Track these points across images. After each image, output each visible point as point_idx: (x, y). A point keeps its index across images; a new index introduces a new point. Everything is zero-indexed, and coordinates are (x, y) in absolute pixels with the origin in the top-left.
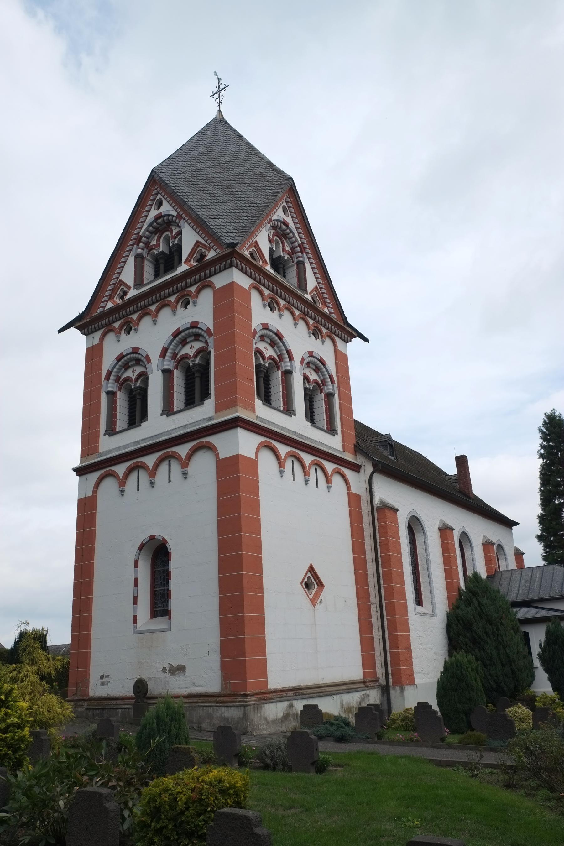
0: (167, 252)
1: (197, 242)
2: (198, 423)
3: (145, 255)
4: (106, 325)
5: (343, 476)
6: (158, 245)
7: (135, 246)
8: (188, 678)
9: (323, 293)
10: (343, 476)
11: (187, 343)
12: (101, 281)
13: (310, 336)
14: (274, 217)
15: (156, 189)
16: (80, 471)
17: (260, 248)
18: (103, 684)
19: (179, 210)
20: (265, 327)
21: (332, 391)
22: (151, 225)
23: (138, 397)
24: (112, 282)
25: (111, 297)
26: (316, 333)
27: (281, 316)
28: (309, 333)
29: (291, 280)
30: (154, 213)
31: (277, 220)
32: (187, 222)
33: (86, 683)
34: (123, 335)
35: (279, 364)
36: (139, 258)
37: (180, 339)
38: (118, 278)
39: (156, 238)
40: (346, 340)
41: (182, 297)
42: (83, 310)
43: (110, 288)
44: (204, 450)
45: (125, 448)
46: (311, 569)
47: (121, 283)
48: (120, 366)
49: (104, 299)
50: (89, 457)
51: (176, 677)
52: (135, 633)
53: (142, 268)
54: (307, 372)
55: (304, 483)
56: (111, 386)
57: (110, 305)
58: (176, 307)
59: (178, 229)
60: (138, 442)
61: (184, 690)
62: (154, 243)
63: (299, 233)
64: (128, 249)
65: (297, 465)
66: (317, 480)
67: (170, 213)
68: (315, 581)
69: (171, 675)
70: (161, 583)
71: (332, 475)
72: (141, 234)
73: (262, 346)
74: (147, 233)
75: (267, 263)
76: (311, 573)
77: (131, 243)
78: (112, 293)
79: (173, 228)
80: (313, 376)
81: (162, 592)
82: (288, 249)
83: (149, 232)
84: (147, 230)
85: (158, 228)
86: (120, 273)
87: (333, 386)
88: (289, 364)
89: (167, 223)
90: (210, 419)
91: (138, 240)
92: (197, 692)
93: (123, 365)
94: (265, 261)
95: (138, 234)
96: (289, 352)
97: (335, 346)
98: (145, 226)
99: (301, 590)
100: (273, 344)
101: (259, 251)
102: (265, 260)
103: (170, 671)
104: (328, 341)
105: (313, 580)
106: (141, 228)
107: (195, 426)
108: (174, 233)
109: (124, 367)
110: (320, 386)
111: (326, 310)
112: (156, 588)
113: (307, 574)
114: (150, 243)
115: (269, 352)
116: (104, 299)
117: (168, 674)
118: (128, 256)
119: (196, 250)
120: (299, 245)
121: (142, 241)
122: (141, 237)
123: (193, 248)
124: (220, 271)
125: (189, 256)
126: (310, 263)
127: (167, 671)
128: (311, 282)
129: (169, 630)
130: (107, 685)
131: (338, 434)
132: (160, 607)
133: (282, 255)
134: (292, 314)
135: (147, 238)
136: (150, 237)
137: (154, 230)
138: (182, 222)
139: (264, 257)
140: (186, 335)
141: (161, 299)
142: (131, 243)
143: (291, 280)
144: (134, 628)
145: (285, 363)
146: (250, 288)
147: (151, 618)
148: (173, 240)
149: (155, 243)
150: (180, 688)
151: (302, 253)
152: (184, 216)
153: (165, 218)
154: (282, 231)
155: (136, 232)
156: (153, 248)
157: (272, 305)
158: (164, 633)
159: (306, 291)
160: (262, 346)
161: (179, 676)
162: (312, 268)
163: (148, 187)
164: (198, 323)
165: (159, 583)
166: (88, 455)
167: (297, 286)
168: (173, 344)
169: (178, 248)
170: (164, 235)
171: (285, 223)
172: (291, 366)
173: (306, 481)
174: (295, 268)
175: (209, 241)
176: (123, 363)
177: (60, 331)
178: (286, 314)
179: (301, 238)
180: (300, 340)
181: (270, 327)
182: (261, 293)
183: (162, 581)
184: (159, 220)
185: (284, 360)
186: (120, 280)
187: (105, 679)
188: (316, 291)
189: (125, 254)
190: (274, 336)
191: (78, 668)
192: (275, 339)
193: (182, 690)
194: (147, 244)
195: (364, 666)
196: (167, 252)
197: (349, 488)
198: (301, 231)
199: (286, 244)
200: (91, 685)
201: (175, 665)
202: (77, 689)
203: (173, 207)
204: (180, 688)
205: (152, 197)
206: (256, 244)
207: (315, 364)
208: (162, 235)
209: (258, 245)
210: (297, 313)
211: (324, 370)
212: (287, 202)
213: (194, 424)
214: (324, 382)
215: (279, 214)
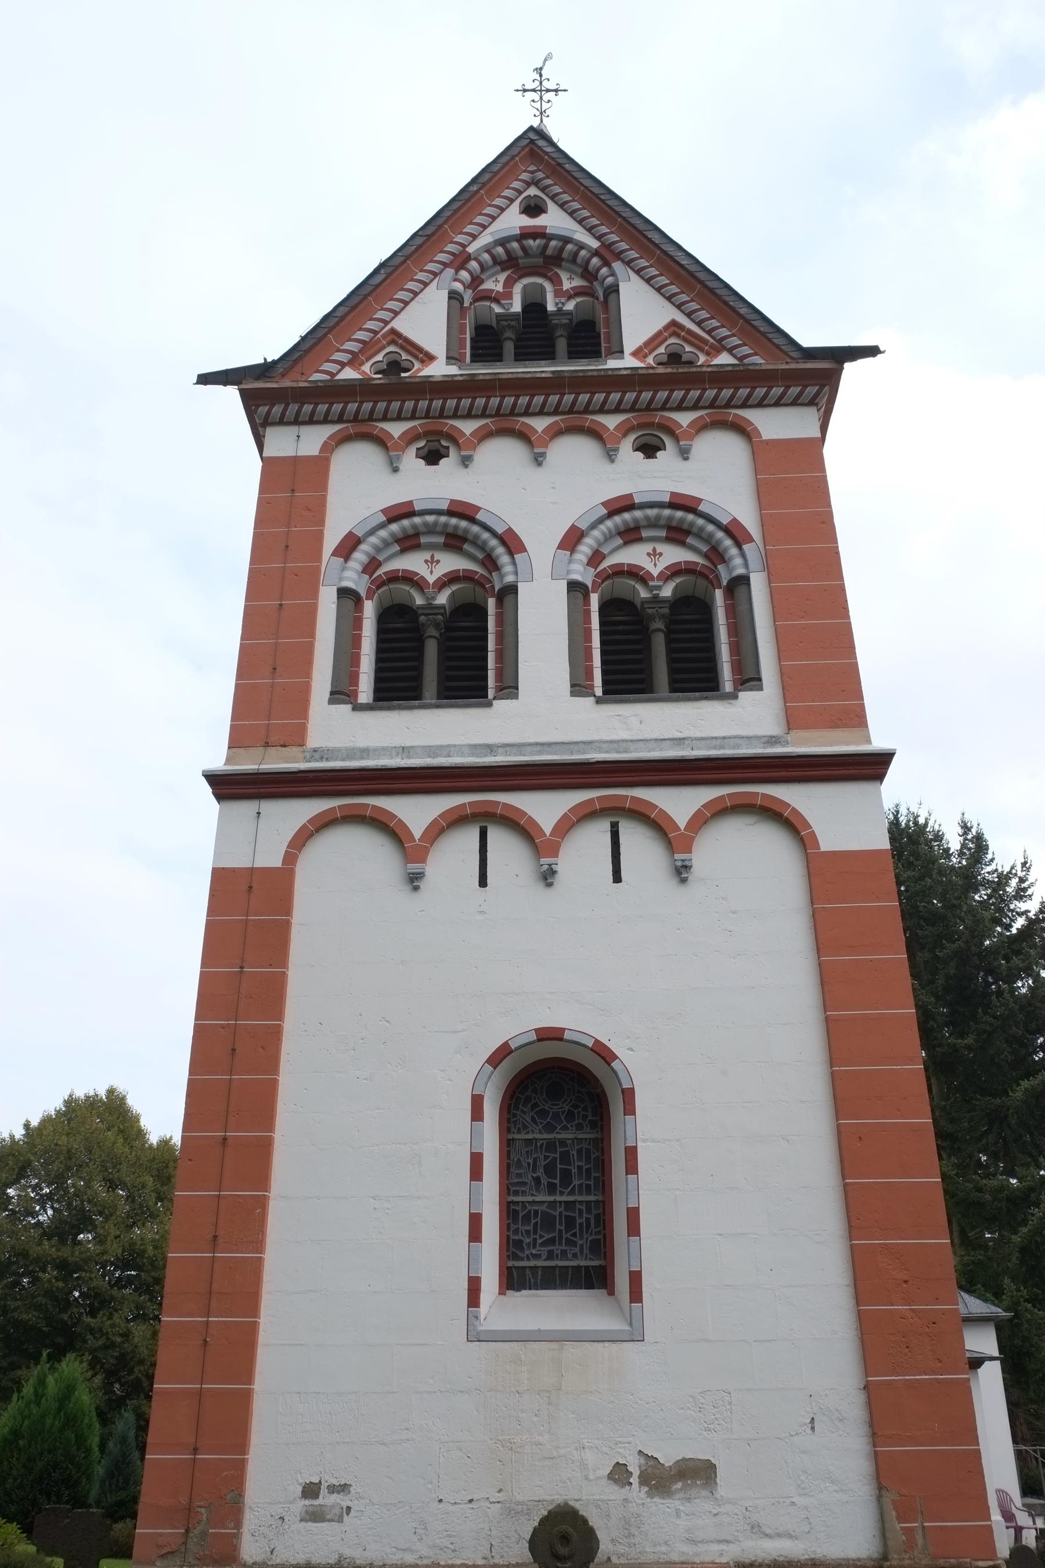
2: (732, 742)
4: (356, 419)
8: (728, 1508)
11: (640, 540)
12: (343, 310)
16: (225, 786)
18: (315, 1516)
22: (503, 242)
23: (432, 631)
24: (370, 325)
25: (355, 361)
30: (513, 221)
33: (232, 1508)
34: (411, 461)
37: (625, 522)
41: (641, 426)
42: (274, 355)
43: (360, 335)
44: (750, 819)
45: (435, 755)
48: (393, 535)
49: (338, 356)
50: (272, 751)
51: (674, 1503)
52: (474, 1336)
56: (353, 578)
57: (349, 374)
60: (491, 748)
61: (715, 1547)
69: (650, 1495)
70: (537, 1180)
72: (471, 249)
74: (486, 257)
77: (442, 257)
78: (361, 351)
81: (544, 1207)
83: (493, 257)
84: (488, 249)
85: (517, 258)
86: (396, 313)
89: (546, 257)
90: (772, 740)
91: (461, 261)
92: (774, 1555)
93: (400, 535)
95: (464, 246)
103: (644, 1480)
106: (474, 237)
107: (722, 747)
109: (449, 535)
112: (516, 1193)
114: (482, 282)
116: (338, 356)
117: (636, 1492)
121: (468, 266)
122: (469, 258)
123: (659, 333)
124: (778, 403)
125: (647, 344)
127: (634, 1480)
129: (635, 1336)
130: (340, 1520)
132: (537, 1257)
135: (483, 268)
136: (488, 268)
140: (647, 518)
141: (571, 411)
142: (442, 257)
144: (472, 1319)
147: (502, 1293)
150: (693, 1542)
153: (553, 243)
155: (460, 238)
158: (615, 1347)
161: (689, 1500)
165: (528, 1179)
166: (267, 745)
168: (602, 527)
170: (539, 280)
176: (404, 530)
177: (205, 379)
183: (540, 1173)
184: (531, 242)
187: (326, 1499)
189: (421, 276)
191: (195, 1451)
193: (702, 1548)
194: (476, 281)
195: (886, 1475)
200: (251, 1520)
201: (668, 1456)
202: (187, 1531)
204: (693, 1542)
205: (516, 184)
213: (718, 743)
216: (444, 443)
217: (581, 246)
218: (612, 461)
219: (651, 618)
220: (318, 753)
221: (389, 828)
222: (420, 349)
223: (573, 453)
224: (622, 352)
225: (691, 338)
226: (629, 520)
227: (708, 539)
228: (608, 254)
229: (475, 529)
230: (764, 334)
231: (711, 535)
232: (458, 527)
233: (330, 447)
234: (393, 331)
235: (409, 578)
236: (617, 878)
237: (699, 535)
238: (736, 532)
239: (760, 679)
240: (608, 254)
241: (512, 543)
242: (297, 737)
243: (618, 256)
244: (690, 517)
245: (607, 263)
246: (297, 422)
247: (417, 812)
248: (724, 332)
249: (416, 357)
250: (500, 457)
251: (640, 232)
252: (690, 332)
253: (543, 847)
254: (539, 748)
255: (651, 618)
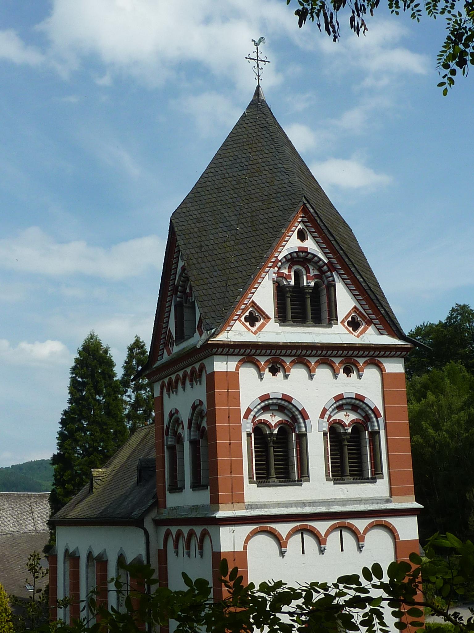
91: (275, 265)
184: (301, 253)
216: (278, 366)
217: (320, 260)
218: (336, 378)
219: (344, 440)
220: (250, 507)
221: (276, 536)
222: (264, 313)
223: (323, 373)
224: (337, 320)
225: (361, 314)
226: (342, 403)
227: (366, 412)
228: (331, 267)
229: (291, 406)
230: (389, 324)
231: (367, 411)
232: (284, 405)
233: (237, 368)
234: (253, 302)
235: (265, 423)
236: (342, 550)
237: (363, 409)
238: (375, 411)
239: (382, 474)
240: (331, 267)
241: (304, 415)
242: (241, 499)
243: (335, 269)
244: (361, 403)
245: (329, 270)
246: (226, 354)
247: (283, 529)
248: (373, 317)
249: (262, 316)
250: (298, 373)
251: (347, 265)
252: (360, 312)
253: (320, 541)
254: (319, 504)
255: (344, 440)
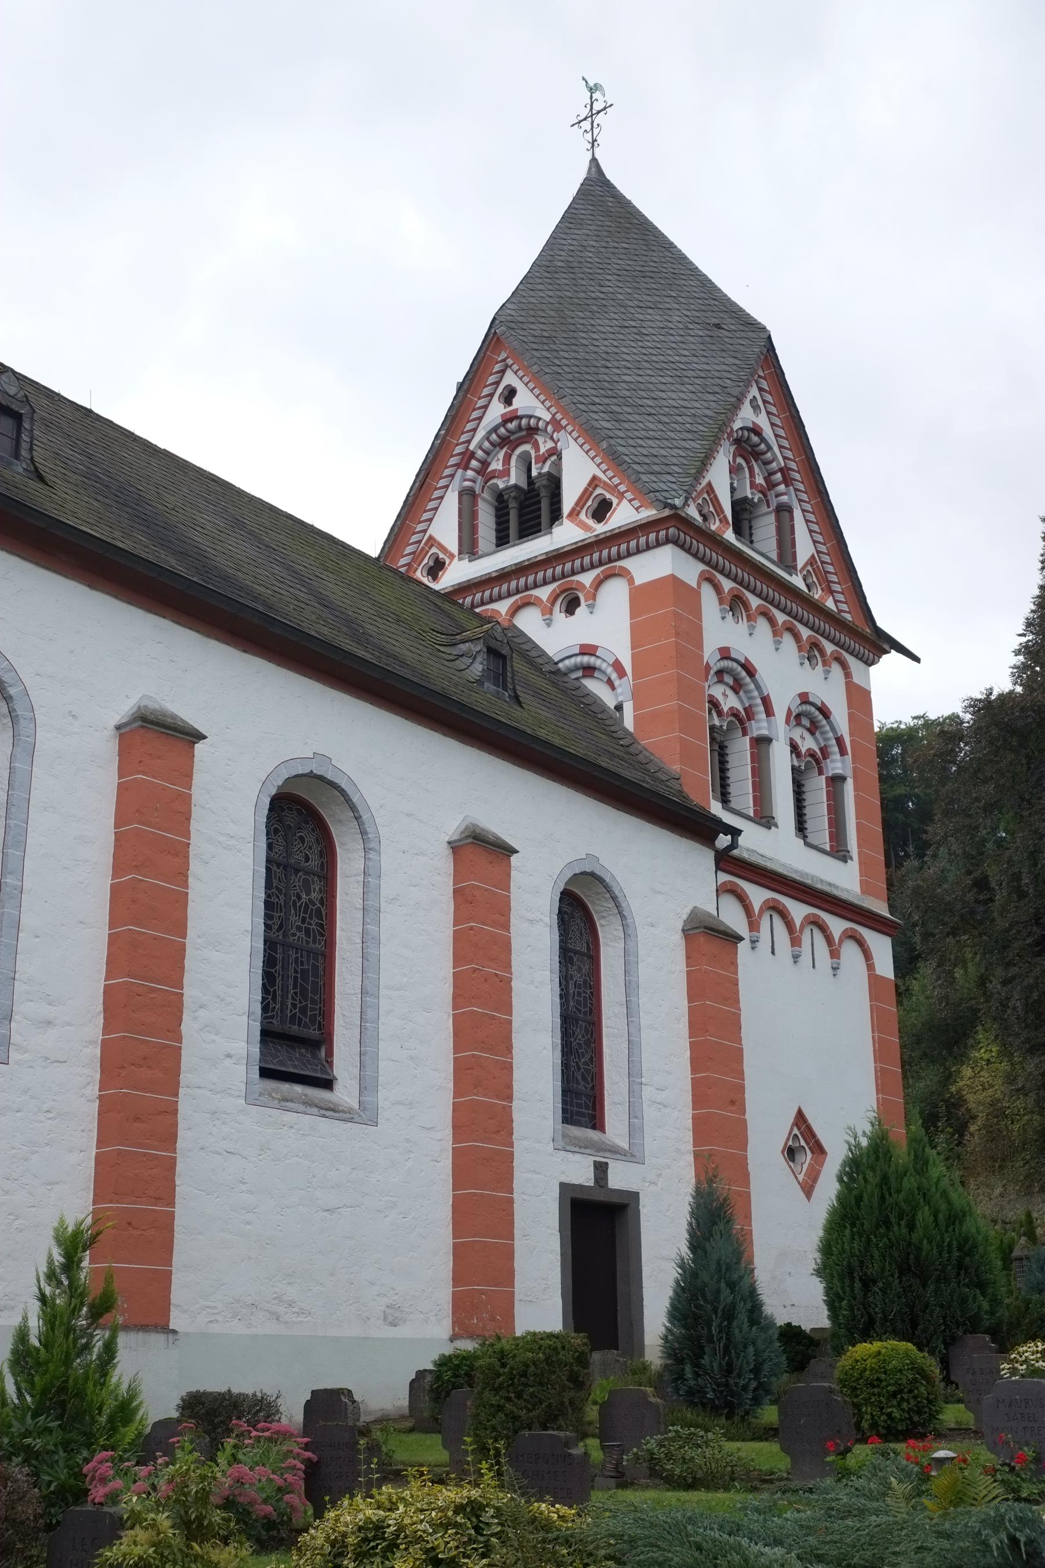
0: (524, 484)
1: (594, 478)
3: (478, 491)
5: (861, 943)
6: (506, 473)
7: (460, 471)
9: (822, 562)
10: (861, 943)
13: (802, 664)
14: (737, 425)
15: (504, 360)
17: (716, 496)
19: (553, 410)
20: (725, 653)
21: (840, 771)
26: (811, 652)
27: (752, 628)
28: (802, 657)
29: (764, 546)
31: (741, 429)
32: (570, 434)
35: (747, 724)
36: (468, 497)
38: (425, 531)
39: (501, 455)
40: (870, 662)
43: (409, 549)
46: (800, 1118)
47: (432, 541)
53: (474, 515)
54: (797, 733)
55: (791, 960)
58: (551, 612)
59: (550, 444)
62: (496, 465)
63: (780, 447)
64: (447, 472)
65: (778, 921)
66: (812, 945)
67: (537, 414)
68: (808, 1144)
71: (841, 941)
73: (718, 691)
75: (727, 522)
76: (799, 1129)
79: (540, 439)
80: (807, 743)
82: (760, 480)
83: (491, 443)
87: (843, 762)
88: (765, 724)
94: (724, 520)
96: (766, 701)
97: (848, 675)
98: (481, 434)
99: (781, 1161)
100: (737, 687)
101: (716, 502)
102: (725, 517)
104: (836, 669)
105: (803, 1143)
108: (543, 450)
110: (817, 760)
111: (830, 604)
113: (791, 1130)
115: (730, 702)
118: (447, 487)
119: (592, 493)
120: (781, 470)
123: (586, 490)
125: (577, 504)
126: (803, 511)
128: (804, 549)
131: (851, 858)
133: (750, 496)
134: (772, 621)
137: (499, 440)
138: (560, 435)
139: (723, 512)
143: (764, 546)
145: (758, 721)
146: (699, 585)
148: (540, 465)
149: (500, 467)
151: (787, 486)
152: (564, 422)
154: (751, 446)
156: (494, 475)
157: (735, 604)
159: (795, 568)
160: (718, 691)
162: (807, 521)
163: (485, 353)
164: (596, 647)
167: (775, 558)
169: (555, 483)
171: (756, 431)
172: (769, 728)
173: (796, 958)
174: (772, 518)
175: (610, 473)
178: (762, 624)
179: (785, 458)
180: (784, 673)
181: (733, 655)
182: (717, 588)
185: (757, 717)
186: (431, 538)
188: (811, 565)
190: (740, 669)
192: (739, 673)
196: (524, 484)
197: (870, 967)
198: (786, 443)
199: (757, 470)
203: (543, 403)
206: (710, 489)
207: (810, 715)
208: (513, 451)
209: (713, 491)
210: (781, 618)
211: (828, 728)
212: (761, 389)
214: (825, 752)
215: (746, 416)
